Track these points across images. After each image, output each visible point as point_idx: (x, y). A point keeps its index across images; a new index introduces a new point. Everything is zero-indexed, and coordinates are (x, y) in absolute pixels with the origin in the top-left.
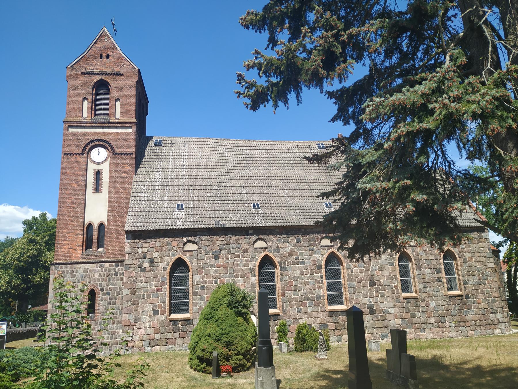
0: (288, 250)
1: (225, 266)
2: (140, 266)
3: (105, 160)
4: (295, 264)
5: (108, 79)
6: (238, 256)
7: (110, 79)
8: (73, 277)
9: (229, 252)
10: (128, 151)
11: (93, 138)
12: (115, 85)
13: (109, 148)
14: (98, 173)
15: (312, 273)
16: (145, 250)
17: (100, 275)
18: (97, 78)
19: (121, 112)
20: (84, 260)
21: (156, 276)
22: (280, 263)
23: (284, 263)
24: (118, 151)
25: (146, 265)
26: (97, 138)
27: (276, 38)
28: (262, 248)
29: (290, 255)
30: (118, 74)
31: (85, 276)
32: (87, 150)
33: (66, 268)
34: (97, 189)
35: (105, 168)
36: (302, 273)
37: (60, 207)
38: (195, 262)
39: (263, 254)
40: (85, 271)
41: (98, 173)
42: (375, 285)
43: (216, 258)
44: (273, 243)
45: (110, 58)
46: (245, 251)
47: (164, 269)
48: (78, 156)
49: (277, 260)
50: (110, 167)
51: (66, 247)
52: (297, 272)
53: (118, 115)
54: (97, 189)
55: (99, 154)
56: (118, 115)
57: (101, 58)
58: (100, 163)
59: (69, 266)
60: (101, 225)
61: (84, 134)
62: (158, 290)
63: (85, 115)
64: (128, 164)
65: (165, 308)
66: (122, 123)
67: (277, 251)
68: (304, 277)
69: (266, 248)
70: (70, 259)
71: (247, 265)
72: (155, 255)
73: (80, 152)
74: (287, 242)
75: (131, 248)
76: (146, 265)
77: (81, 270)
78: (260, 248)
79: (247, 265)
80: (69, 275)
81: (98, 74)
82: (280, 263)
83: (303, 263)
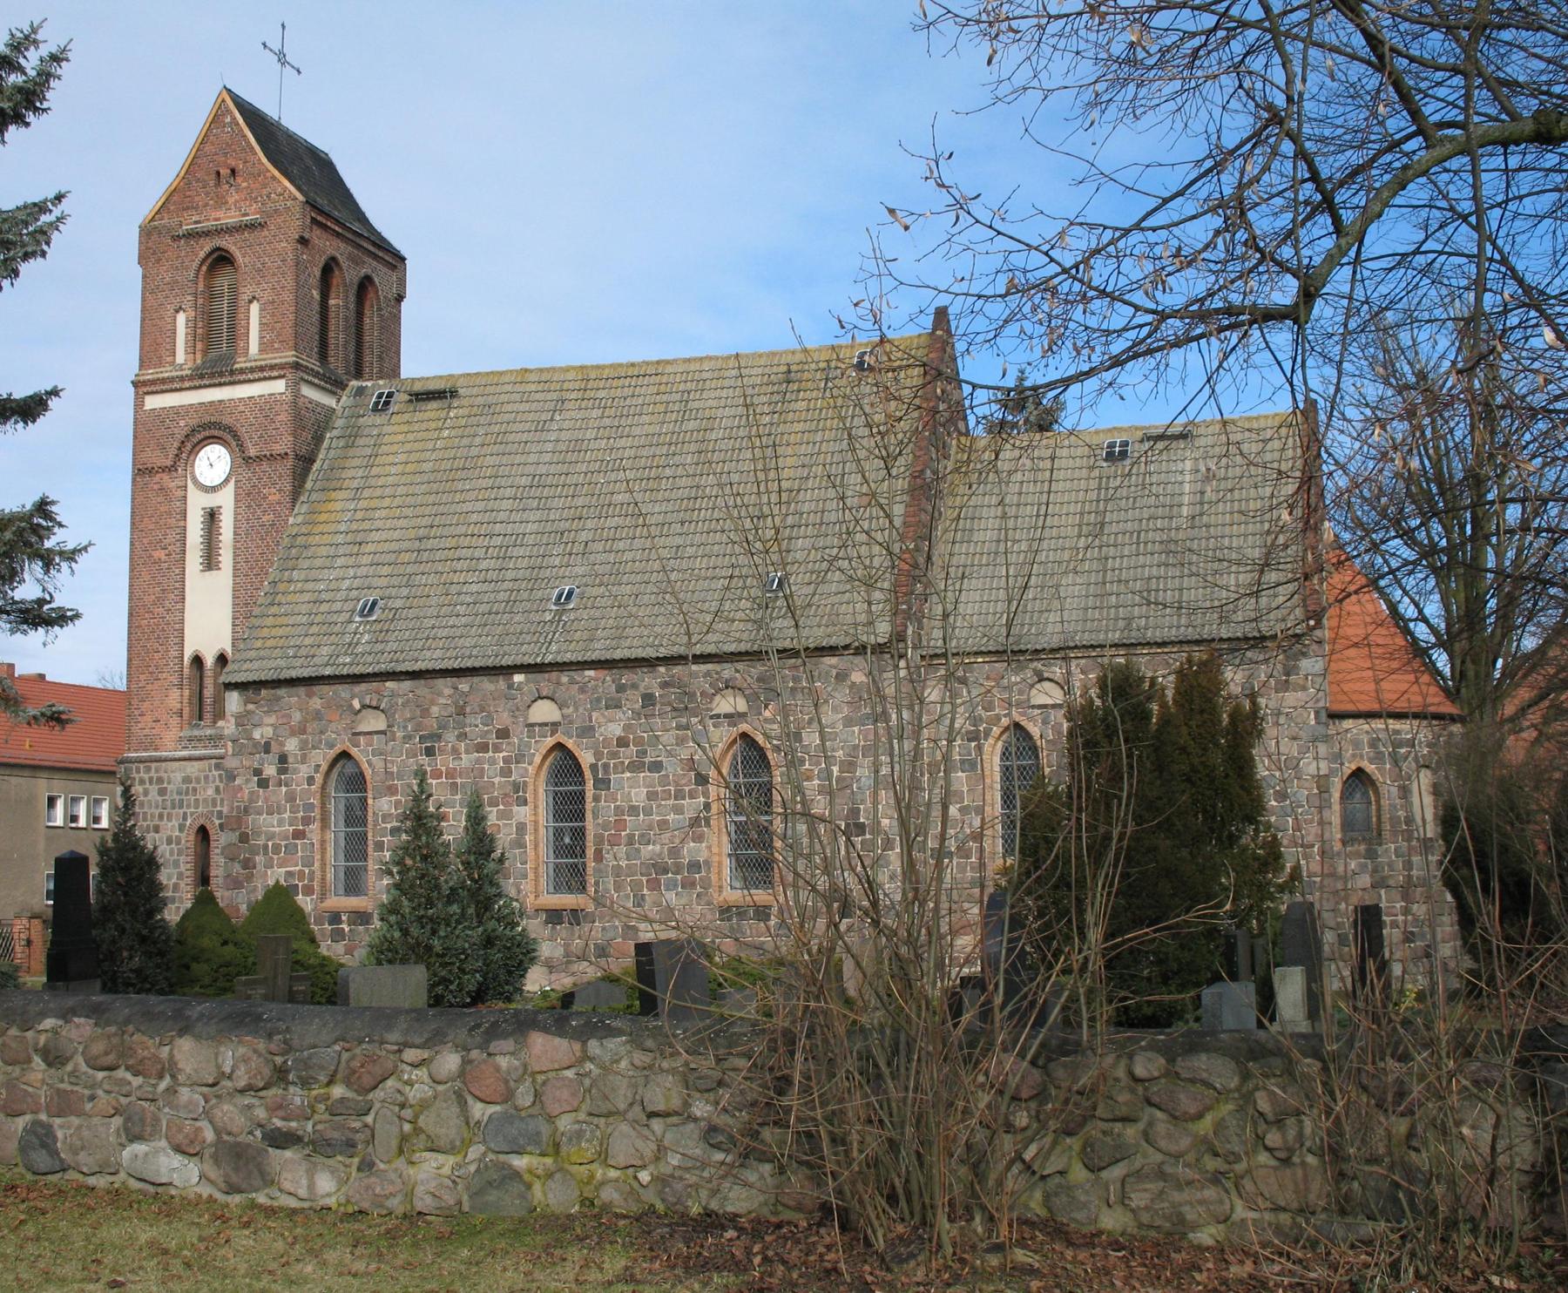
0: (616, 730)
1: (451, 774)
2: (258, 772)
3: (227, 481)
4: (636, 767)
5: (226, 242)
6: (483, 748)
7: (235, 244)
8: (162, 792)
9: (462, 736)
10: (278, 448)
11: (194, 422)
12: (247, 260)
13: (228, 437)
14: (212, 516)
15: (679, 795)
16: (269, 732)
17: (217, 790)
18: (207, 246)
19: (261, 338)
20: (185, 753)
21: (291, 798)
22: (594, 767)
23: (606, 766)
24: (252, 452)
25: (270, 771)
26: (207, 419)
27: (649, 1043)
28: (546, 724)
29: (622, 742)
30: (251, 226)
31: (187, 793)
32: (189, 446)
33: (148, 770)
34: (210, 561)
35: (225, 500)
36: (651, 796)
37: (131, 615)
38: (378, 762)
39: (550, 741)
40: (187, 780)
41: (212, 516)
42: (864, 833)
43: (430, 752)
44: (576, 709)
45: (239, 180)
46: (503, 734)
47: (311, 780)
48: (165, 477)
49: (586, 758)
50: (237, 495)
51: (148, 718)
52: (639, 796)
53: (254, 348)
54: (210, 562)
55: (213, 463)
56: (254, 348)
57: (218, 184)
58: (214, 489)
59: (154, 765)
60: (222, 659)
61: (177, 411)
62: (299, 835)
63: (180, 357)
64: (276, 488)
65: (312, 880)
66: (262, 369)
67: (587, 731)
68: (658, 806)
69: (555, 725)
70: (156, 750)
71: (506, 772)
72: (292, 745)
73: (169, 463)
74: (617, 707)
75: (237, 725)
76: (270, 771)
77: (178, 777)
78: (540, 725)
79: (506, 772)
80: (154, 789)
81: (207, 234)
82: (594, 767)
83: (656, 766)
